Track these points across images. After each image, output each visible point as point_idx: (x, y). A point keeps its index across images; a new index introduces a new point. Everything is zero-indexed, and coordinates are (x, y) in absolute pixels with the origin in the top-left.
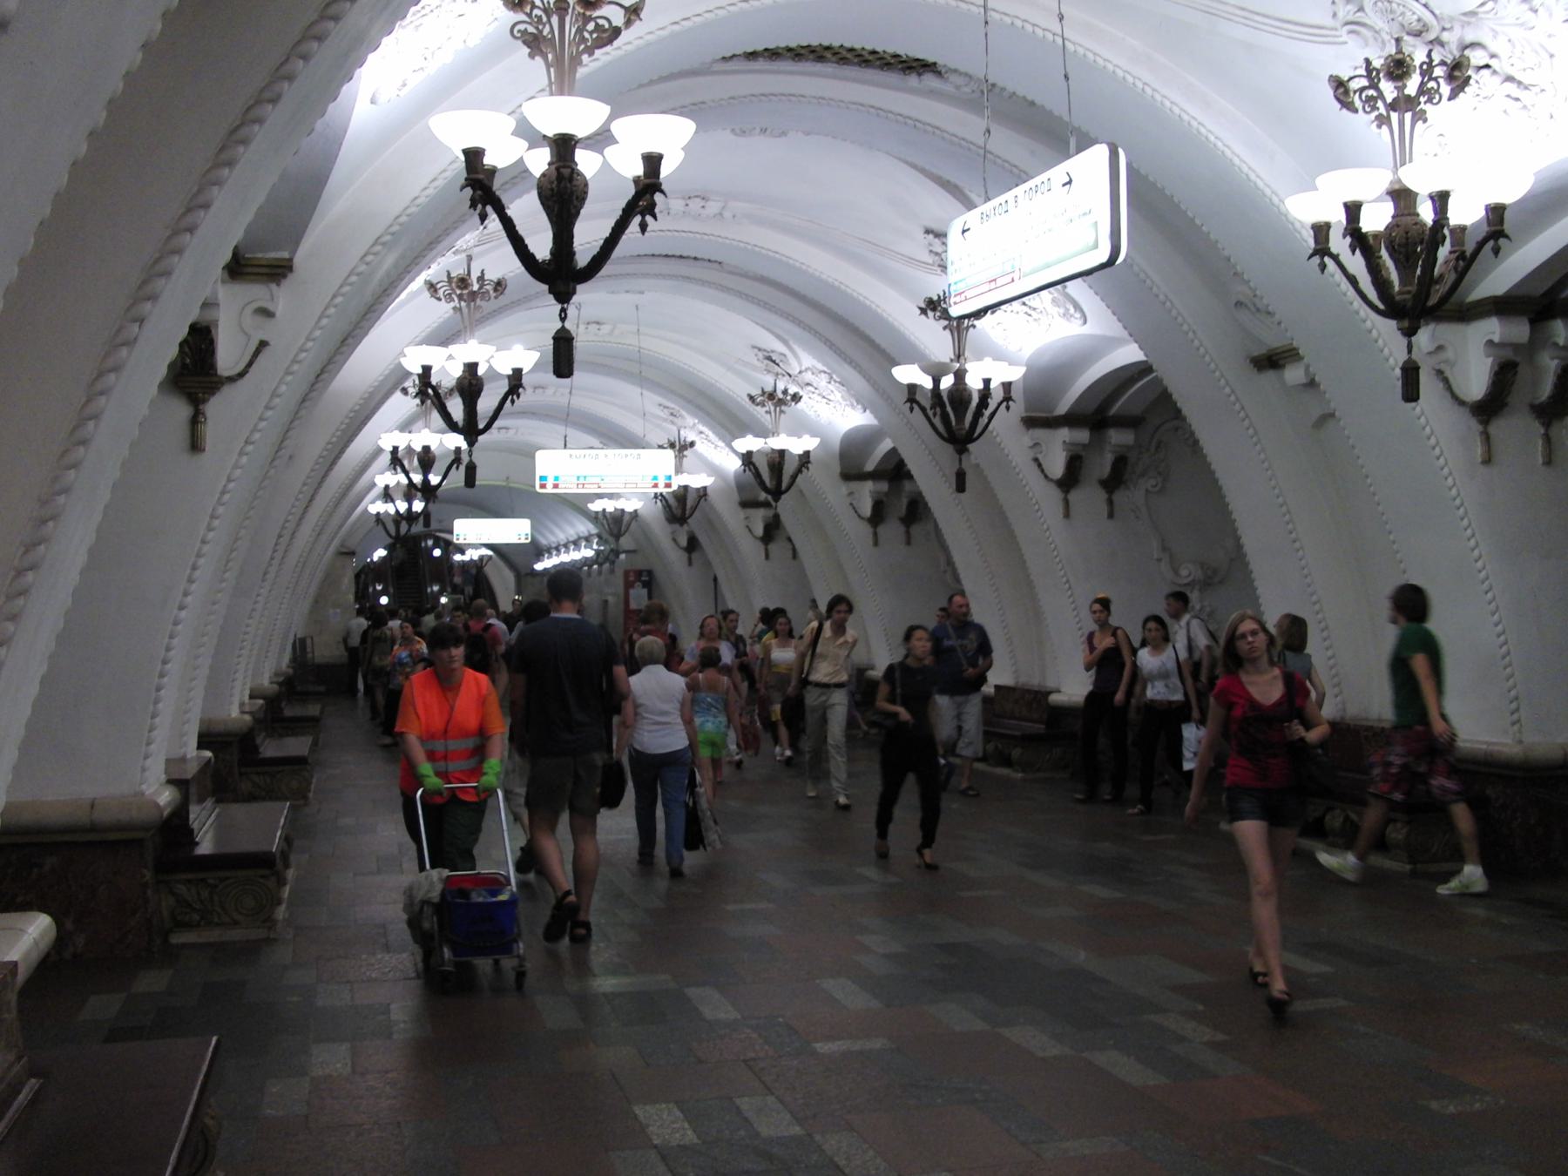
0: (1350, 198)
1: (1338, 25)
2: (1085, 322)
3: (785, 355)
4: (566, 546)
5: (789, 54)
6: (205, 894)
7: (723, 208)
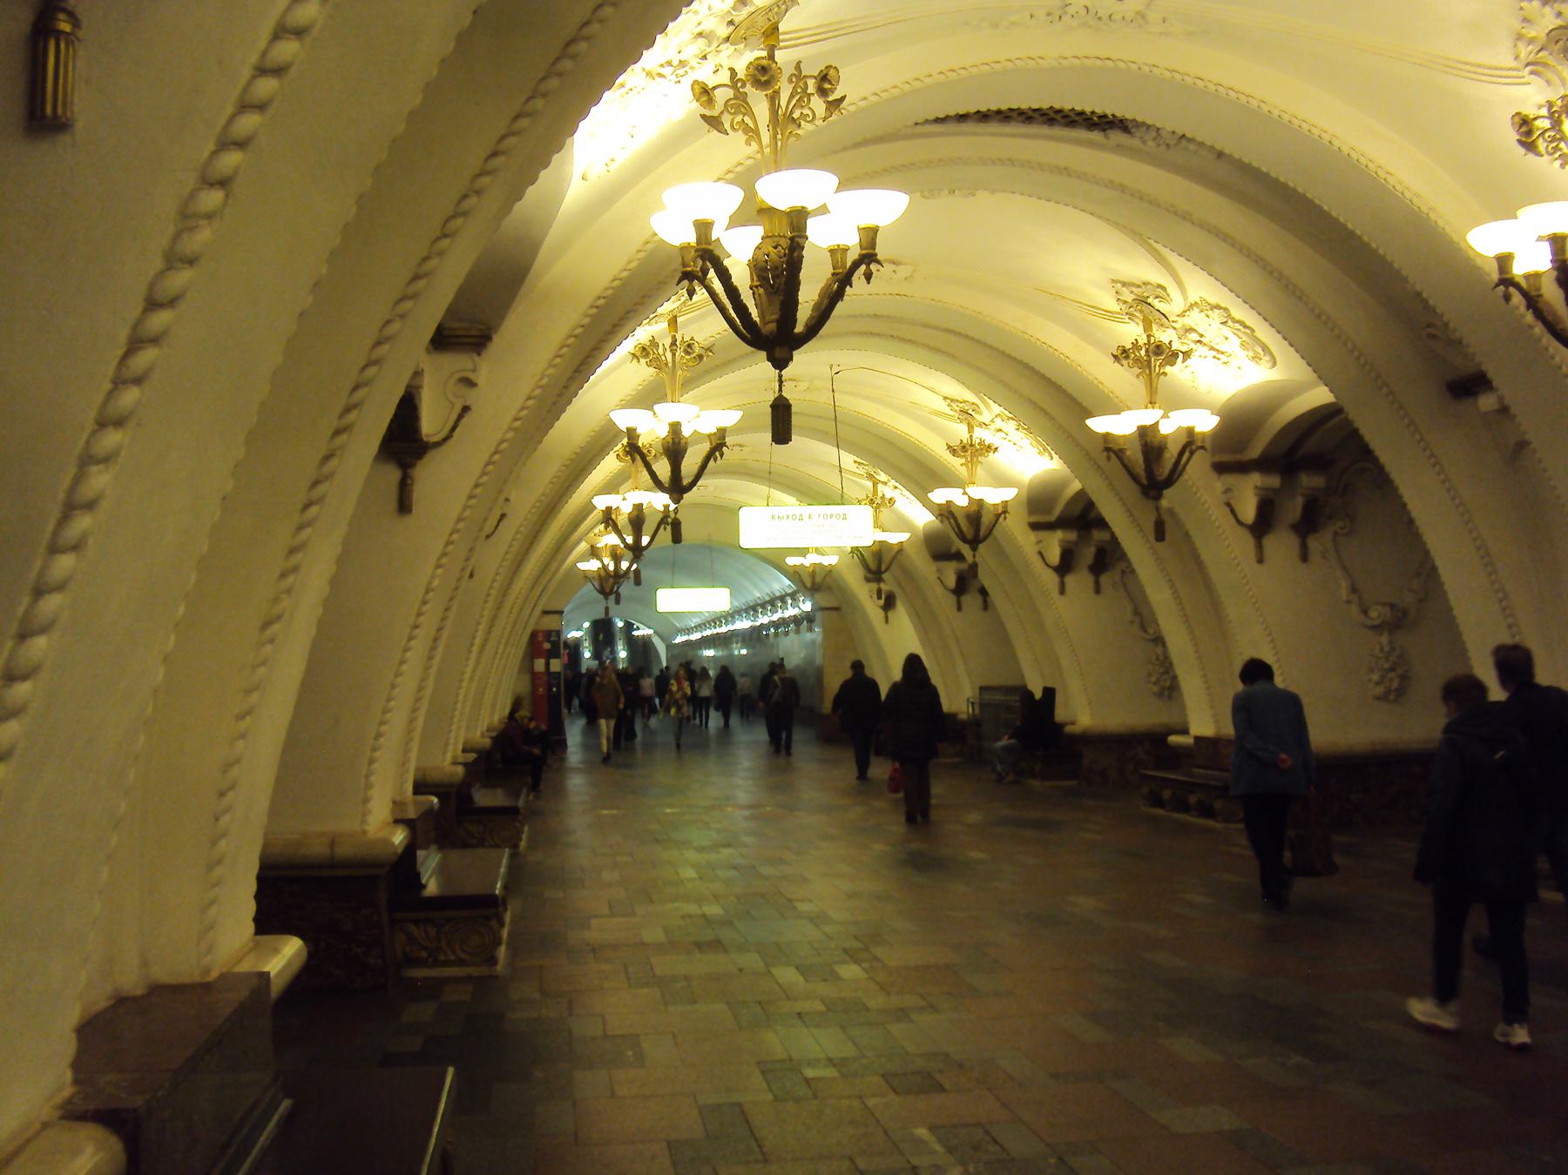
0: (701, 216)
1: (1520, 66)
2: (1052, 458)
3: (976, 405)
5: (1041, 119)
6: (432, 932)
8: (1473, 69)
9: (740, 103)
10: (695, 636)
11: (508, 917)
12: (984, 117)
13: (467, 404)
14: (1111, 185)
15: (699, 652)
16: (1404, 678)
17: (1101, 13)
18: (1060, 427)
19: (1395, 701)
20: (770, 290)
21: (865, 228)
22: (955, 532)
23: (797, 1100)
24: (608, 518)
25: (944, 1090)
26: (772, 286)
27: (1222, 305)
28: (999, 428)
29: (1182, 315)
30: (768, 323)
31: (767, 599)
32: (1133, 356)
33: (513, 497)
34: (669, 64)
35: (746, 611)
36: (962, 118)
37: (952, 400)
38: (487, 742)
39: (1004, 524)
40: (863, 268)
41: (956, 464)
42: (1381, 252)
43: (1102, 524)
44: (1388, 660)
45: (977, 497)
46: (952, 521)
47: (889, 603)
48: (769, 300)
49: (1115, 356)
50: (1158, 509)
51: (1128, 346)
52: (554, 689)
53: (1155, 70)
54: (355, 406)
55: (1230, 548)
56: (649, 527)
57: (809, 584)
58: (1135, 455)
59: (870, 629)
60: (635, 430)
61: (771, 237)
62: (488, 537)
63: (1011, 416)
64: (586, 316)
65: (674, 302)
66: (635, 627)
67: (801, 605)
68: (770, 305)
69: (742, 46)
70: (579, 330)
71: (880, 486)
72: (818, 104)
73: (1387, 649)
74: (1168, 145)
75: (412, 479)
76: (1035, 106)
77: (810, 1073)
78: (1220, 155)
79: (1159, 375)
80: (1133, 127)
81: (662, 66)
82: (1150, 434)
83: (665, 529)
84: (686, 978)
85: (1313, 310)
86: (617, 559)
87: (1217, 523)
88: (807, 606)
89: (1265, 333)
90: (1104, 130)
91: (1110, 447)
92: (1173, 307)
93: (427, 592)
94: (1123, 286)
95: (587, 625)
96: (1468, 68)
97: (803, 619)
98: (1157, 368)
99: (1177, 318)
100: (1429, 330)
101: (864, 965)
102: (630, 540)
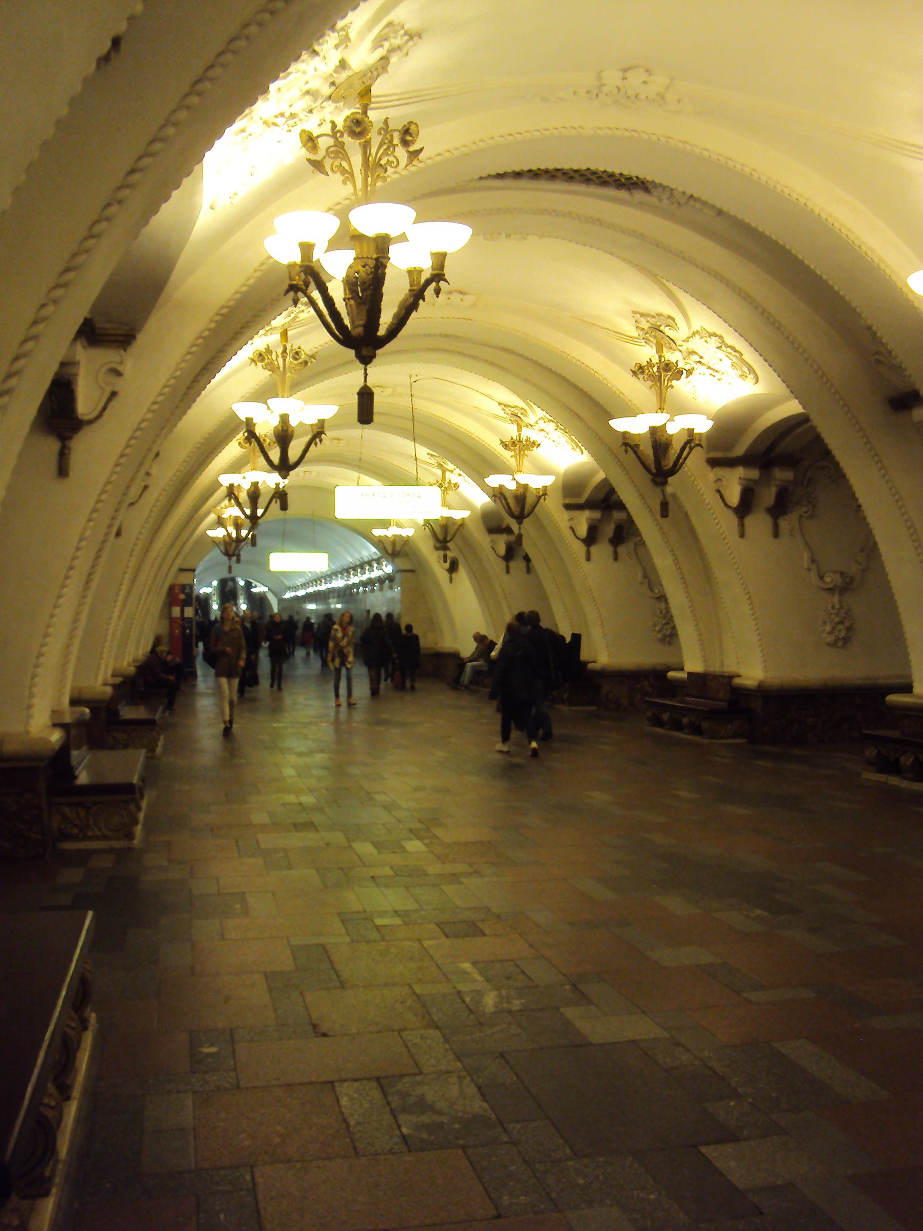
2: (582, 453)
3: (524, 410)
4: (354, 569)
6: (82, 813)
7: (667, 88)
8: (917, 150)
9: (339, 150)
10: (301, 593)
11: (144, 804)
12: (535, 175)
13: (115, 389)
14: (633, 233)
15: (304, 606)
16: (849, 629)
17: (629, 93)
18: (589, 428)
19: (842, 647)
20: (359, 301)
21: (435, 253)
22: (506, 510)
23: (368, 942)
24: (231, 493)
25: (485, 935)
26: (361, 298)
27: (718, 333)
28: (541, 428)
29: (687, 340)
30: (356, 327)
31: (358, 563)
32: (647, 371)
33: (154, 472)
34: (282, 115)
35: (341, 573)
36: (518, 175)
37: (505, 406)
38: (132, 670)
39: (544, 505)
40: (434, 284)
41: (507, 456)
42: (842, 293)
43: (621, 506)
44: (837, 616)
45: (522, 482)
46: (504, 502)
47: (453, 567)
48: (358, 309)
49: (633, 372)
50: (663, 493)
51: (644, 364)
52: (188, 631)
53: (670, 141)
54: (16, 373)
55: (719, 526)
56: (263, 501)
57: (390, 551)
58: (647, 450)
59: (438, 585)
60: (252, 419)
61: (360, 258)
62: (131, 504)
63: (551, 418)
64: (211, 321)
65: (285, 318)
66: (253, 585)
67: (384, 568)
68: (359, 313)
69: (341, 104)
70: (206, 333)
71: (447, 474)
72: (401, 153)
73: (837, 606)
74: (679, 204)
75: (69, 449)
76: (575, 167)
77: (379, 921)
78: (720, 212)
79: (667, 387)
80: (653, 187)
81: (276, 116)
82: (659, 434)
83: (276, 502)
84: (285, 850)
85: (788, 338)
86: (238, 527)
87: (709, 506)
88: (389, 569)
89: (750, 356)
90: (629, 190)
91: (628, 443)
92: (679, 333)
93: (80, 540)
94: (641, 317)
95: (215, 583)
96: (913, 149)
97: (386, 579)
98: (666, 382)
99: (683, 343)
100: (878, 357)
101: (425, 841)
102: (248, 512)
